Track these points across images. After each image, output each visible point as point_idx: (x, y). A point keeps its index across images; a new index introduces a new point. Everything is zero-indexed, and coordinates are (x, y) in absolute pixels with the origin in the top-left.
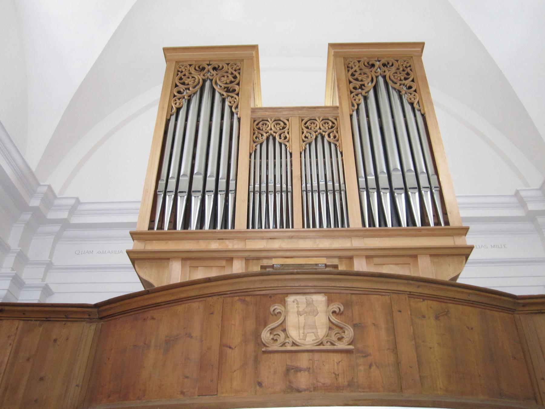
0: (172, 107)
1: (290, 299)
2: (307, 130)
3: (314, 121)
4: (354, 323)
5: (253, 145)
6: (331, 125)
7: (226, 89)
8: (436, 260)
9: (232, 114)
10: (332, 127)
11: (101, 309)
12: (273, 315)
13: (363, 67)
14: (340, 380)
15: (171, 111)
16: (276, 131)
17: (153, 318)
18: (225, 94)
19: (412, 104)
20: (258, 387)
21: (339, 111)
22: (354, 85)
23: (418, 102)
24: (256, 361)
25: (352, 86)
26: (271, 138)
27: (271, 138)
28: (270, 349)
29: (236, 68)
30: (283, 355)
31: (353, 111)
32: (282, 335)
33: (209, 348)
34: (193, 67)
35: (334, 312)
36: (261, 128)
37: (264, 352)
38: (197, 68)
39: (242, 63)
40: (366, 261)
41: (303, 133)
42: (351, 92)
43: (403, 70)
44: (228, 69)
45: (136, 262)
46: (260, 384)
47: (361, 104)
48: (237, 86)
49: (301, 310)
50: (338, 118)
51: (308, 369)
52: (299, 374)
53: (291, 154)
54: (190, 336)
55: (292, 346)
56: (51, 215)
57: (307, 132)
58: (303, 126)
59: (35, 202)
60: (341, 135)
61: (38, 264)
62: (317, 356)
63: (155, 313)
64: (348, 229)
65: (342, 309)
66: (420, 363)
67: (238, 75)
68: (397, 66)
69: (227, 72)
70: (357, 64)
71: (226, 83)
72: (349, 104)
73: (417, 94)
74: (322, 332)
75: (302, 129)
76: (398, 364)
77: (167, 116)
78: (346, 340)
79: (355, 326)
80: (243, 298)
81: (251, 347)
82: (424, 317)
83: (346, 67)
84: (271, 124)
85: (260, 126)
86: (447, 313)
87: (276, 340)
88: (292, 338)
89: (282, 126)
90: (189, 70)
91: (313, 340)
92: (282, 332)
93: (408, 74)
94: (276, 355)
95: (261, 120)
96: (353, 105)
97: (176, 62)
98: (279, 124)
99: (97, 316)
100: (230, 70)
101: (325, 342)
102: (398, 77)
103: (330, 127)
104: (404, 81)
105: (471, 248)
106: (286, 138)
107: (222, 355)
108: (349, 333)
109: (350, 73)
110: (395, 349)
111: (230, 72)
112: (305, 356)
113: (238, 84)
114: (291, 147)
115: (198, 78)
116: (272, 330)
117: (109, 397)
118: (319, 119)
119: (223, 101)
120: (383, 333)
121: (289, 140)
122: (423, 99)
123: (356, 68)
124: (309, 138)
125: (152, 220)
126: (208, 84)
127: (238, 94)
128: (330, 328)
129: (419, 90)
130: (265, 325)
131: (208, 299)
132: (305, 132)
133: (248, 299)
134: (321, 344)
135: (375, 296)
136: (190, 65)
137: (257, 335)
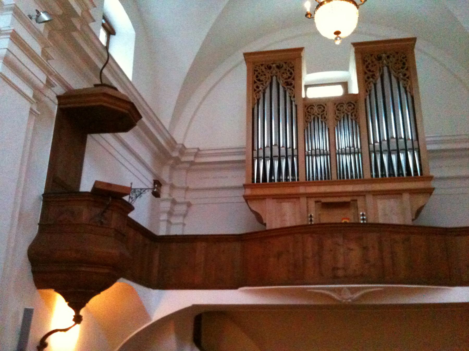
10: (354, 109)
19: (405, 88)
23: (410, 86)
31: (367, 95)
36: (310, 112)
38: (266, 67)
52: (339, 271)
54: (288, 251)
56: (184, 159)
59: (175, 154)
61: (182, 188)
96: (367, 91)
104: (402, 69)
105: (434, 189)
106: (325, 118)
110: (382, 259)
113: (293, 79)
114: (328, 124)
123: (369, 61)
126: (274, 78)
133: (314, 235)
136: (262, 65)
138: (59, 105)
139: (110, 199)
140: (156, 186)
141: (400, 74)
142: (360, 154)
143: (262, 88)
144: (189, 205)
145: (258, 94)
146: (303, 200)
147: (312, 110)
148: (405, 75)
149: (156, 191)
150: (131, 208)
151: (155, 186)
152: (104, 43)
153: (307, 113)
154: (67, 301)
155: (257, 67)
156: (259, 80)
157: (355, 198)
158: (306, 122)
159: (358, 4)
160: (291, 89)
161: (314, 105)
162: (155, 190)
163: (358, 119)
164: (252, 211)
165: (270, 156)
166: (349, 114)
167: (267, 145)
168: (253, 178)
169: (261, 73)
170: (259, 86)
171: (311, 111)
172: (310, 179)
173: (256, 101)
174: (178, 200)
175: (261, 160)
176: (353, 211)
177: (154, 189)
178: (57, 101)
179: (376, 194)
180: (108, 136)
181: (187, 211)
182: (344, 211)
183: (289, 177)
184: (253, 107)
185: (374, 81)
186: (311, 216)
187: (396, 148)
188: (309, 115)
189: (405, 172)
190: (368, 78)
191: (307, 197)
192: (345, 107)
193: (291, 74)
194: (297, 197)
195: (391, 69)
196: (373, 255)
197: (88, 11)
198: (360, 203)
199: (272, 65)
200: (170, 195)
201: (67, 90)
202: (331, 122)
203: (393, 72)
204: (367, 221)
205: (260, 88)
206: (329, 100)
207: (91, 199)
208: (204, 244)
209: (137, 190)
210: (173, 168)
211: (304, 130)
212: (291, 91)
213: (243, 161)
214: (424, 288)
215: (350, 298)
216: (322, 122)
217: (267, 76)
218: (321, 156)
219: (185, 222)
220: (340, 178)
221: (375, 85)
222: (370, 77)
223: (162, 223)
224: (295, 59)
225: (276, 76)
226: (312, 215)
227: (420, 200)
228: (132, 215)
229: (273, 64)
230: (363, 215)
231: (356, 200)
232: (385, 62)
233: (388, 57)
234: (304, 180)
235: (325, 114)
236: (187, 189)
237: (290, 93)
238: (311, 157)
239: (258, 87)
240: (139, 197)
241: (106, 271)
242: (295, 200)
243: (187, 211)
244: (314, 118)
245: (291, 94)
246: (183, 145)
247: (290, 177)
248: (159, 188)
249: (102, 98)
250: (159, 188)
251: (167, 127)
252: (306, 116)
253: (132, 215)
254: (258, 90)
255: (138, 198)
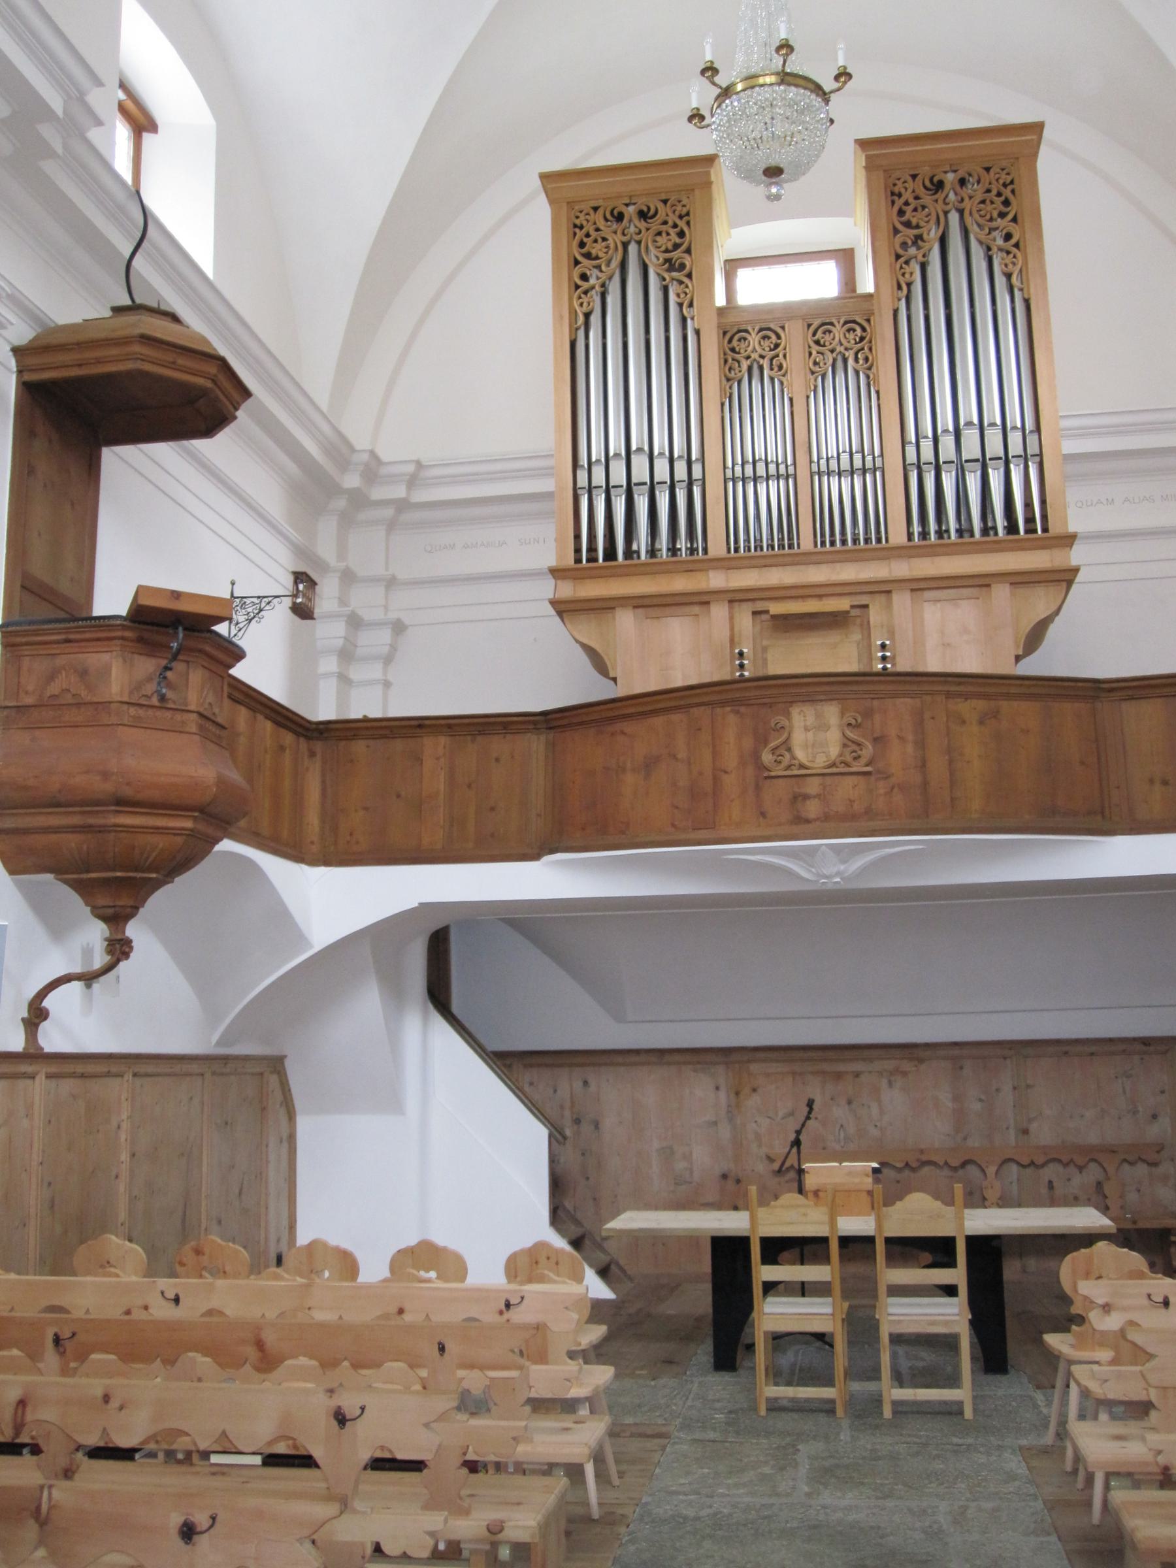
0: (576, 311)
1: (795, 711)
2: (818, 348)
3: (829, 327)
4: (875, 735)
5: (725, 386)
6: (859, 335)
7: (667, 265)
8: (1022, 591)
9: (684, 320)
10: (862, 339)
11: (549, 717)
12: (774, 730)
13: (921, 191)
14: (856, 806)
15: (576, 324)
16: (763, 353)
17: (623, 733)
18: (666, 275)
19: (1008, 276)
20: (761, 819)
21: (874, 302)
22: (902, 238)
23: (1021, 271)
24: (758, 788)
25: (899, 239)
26: (755, 367)
27: (755, 367)
28: (773, 774)
29: (681, 210)
30: (789, 780)
31: (899, 300)
32: (787, 755)
33: (701, 774)
34: (600, 212)
35: (849, 724)
36: (737, 349)
37: (766, 778)
38: (609, 216)
39: (691, 198)
40: (912, 597)
41: (810, 354)
42: (898, 257)
43: (999, 194)
44: (667, 215)
45: (565, 615)
46: (763, 814)
47: (914, 284)
48: (686, 256)
49: (808, 723)
50: (872, 318)
51: (818, 796)
52: (808, 802)
53: (791, 400)
54: (674, 757)
55: (799, 769)
56: (377, 494)
57: (818, 353)
58: (809, 340)
59: (352, 481)
60: (876, 355)
61: (375, 580)
62: (828, 780)
63: (629, 727)
64: (888, 545)
65: (859, 720)
66: (953, 783)
67: (686, 229)
68: (987, 182)
69: (665, 223)
70: (910, 185)
71: (667, 251)
72: (892, 286)
73: (1019, 255)
74: (834, 751)
75: (810, 347)
76: (925, 784)
77: (570, 335)
78: (863, 761)
79: (876, 740)
80: (737, 708)
81: (750, 771)
82: (964, 722)
83: (889, 194)
84: (754, 339)
85: (735, 345)
86: (995, 714)
87: (780, 762)
88: (799, 760)
89: (774, 342)
90: (595, 223)
91: (824, 762)
92: (786, 753)
93: (1006, 203)
94: (781, 780)
95: (735, 330)
96: (899, 287)
97: (568, 203)
98: (769, 338)
99: (545, 726)
100: (672, 218)
101: (838, 764)
102: (987, 212)
103: (858, 340)
104: (999, 220)
105: (1076, 570)
106: (780, 367)
107: (716, 780)
108: (868, 751)
109: (896, 208)
110: (923, 765)
111: (671, 223)
112: (816, 781)
113: (688, 251)
114: (790, 385)
115: (614, 240)
116: (773, 750)
117: (583, 829)
118: (839, 322)
119: (665, 290)
120: (910, 749)
121: (786, 372)
122: (1030, 266)
123: (908, 196)
124: (821, 364)
125: (578, 550)
126: (632, 249)
127: (689, 276)
128: (845, 745)
129: (1025, 242)
130: (766, 742)
131: (692, 710)
132: (814, 353)
133: (743, 709)
134: (833, 765)
135: (902, 700)
136: (595, 209)
137: (756, 755)
138: (20, 372)
139: (181, 635)
140: (301, 587)
141: (995, 234)
142: (878, 474)
143: (598, 278)
144: (399, 628)
145: (585, 299)
146: (719, 612)
147: (743, 345)
148: (1008, 237)
149: (300, 603)
150: (238, 655)
151: (297, 588)
152: (128, 177)
153: (729, 352)
154: (87, 904)
155: (582, 216)
156: (588, 256)
157: (864, 600)
158: (728, 380)
159: (827, 89)
160: (681, 282)
161: (750, 329)
162: (299, 600)
163: (874, 369)
164: (577, 641)
165: (624, 483)
166: (850, 355)
167: (615, 450)
168: (578, 550)
169: (593, 234)
170: (588, 273)
171: (740, 349)
172: (739, 547)
173: (581, 319)
174: (367, 615)
175: (601, 495)
176: (857, 636)
177: (295, 596)
178: (13, 363)
179: (919, 586)
180: (162, 450)
181: (393, 648)
182: (833, 637)
183: (681, 544)
184: (573, 337)
185: (920, 258)
186: (741, 654)
187: (977, 454)
188: (733, 359)
189: (1001, 522)
190: (904, 245)
191: (730, 602)
192: (838, 331)
193: (681, 234)
194: (702, 600)
195: (968, 220)
196: (899, 757)
197: (81, 100)
198: (875, 615)
199: (623, 209)
200: (343, 602)
201: (39, 330)
202: (797, 378)
203: (973, 228)
204: (894, 665)
205: (592, 281)
206: (790, 312)
207: (128, 634)
208: (443, 740)
209: (248, 601)
210: (346, 521)
211: (723, 405)
212: (681, 288)
213: (549, 496)
214: (1070, 840)
215: (838, 874)
216: (772, 379)
217: (611, 242)
218: (770, 482)
219: (390, 678)
220: (823, 543)
221: (923, 267)
222: (910, 243)
223: (322, 684)
224: (690, 190)
225: (639, 243)
226: (745, 650)
227: (1039, 603)
228: (239, 671)
229: (627, 205)
230: (883, 646)
231: (866, 606)
232: (952, 196)
233: (962, 182)
234: (722, 552)
235: (781, 356)
236: (391, 583)
237: (678, 295)
238: (741, 483)
239: (584, 277)
240: (256, 619)
241: (189, 824)
242: (696, 609)
243: (393, 648)
244: (750, 369)
245: (682, 296)
246: (372, 453)
247: (682, 543)
248: (310, 594)
249: (137, 348)
250: (310, 594)
251: (323, 402)
252: (726, 361)
253: (239, 671)
254: (585, 285)
255: (254, 621)
